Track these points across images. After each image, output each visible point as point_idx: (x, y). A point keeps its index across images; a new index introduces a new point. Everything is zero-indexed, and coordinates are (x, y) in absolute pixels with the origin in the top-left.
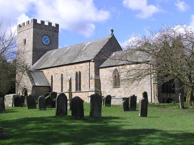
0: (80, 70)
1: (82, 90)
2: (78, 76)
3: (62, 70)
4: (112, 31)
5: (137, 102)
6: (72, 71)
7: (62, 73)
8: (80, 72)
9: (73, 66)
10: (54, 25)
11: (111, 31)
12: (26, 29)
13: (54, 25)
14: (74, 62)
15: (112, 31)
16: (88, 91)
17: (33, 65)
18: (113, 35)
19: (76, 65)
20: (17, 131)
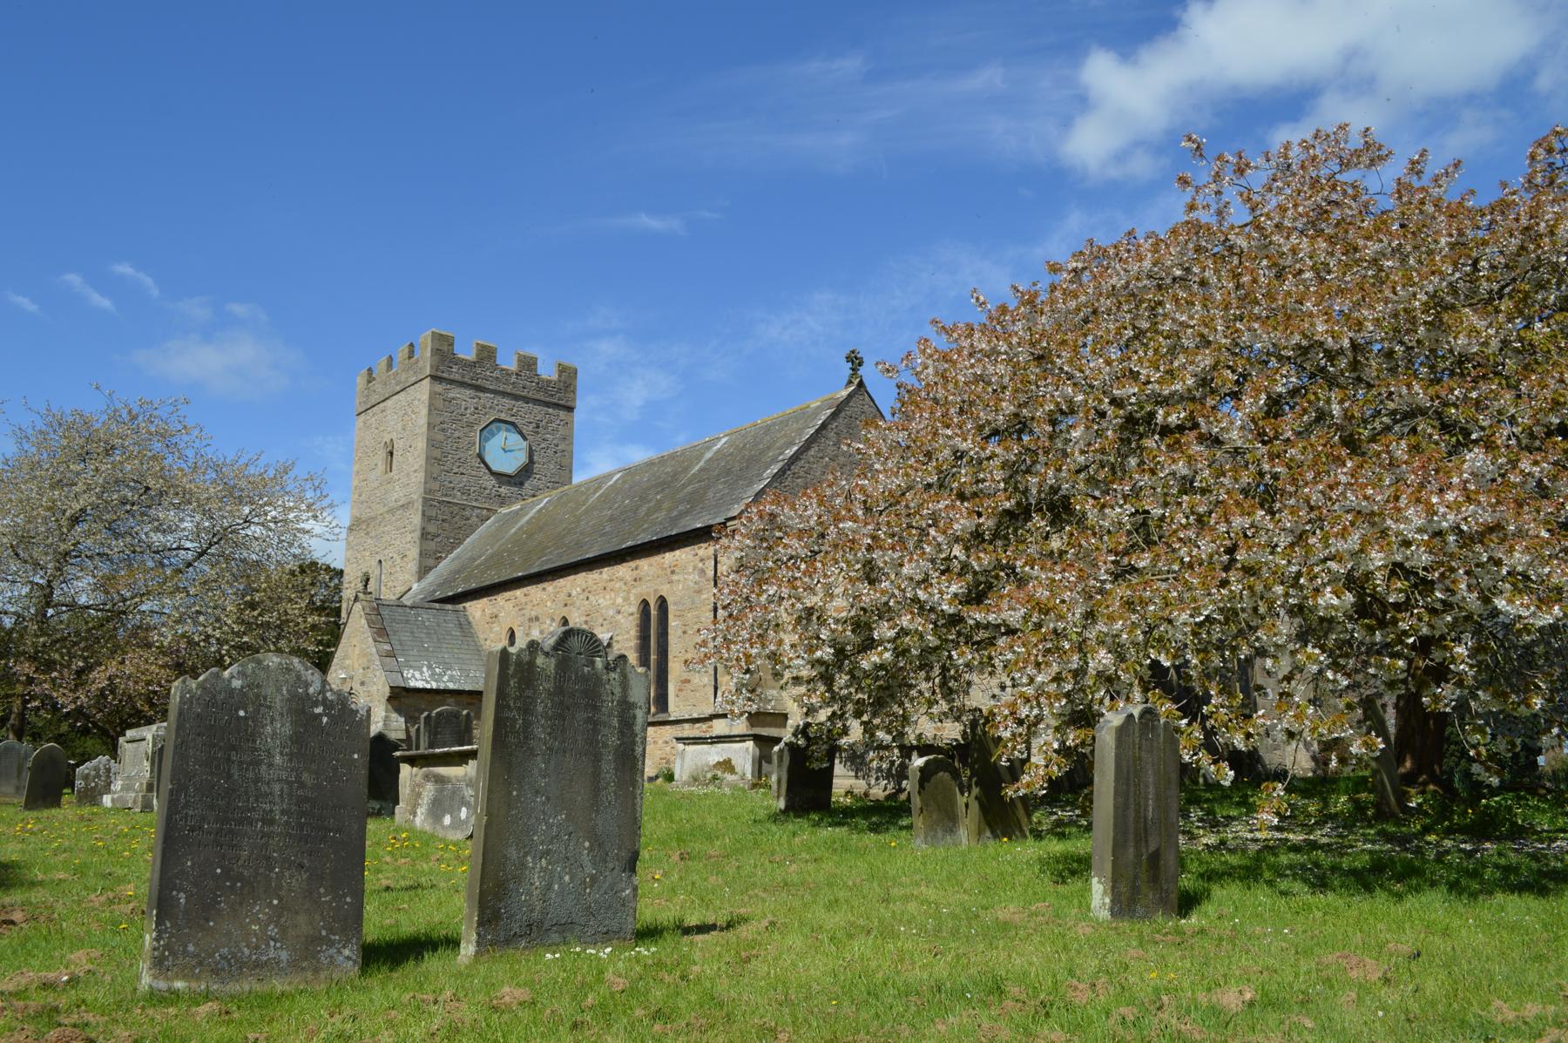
0: (665, 590)
1: (676, 709)
2: (654, 621)
3: (562, 597)
4: (855, 361)
5: (467, 605)
6: (619, 600)
7: (564, 612)
8: (663, 603)
9: (623, 570)
10: (547, 371)
11: (848, 359)
12: (414, 379)
13: (547, 371)
14: (630, 543)
15: (855, 361)
16: (709, 711)
17: (419, 580)
18: (861, 384)
19: (534, 591)
20: (517, 515)
